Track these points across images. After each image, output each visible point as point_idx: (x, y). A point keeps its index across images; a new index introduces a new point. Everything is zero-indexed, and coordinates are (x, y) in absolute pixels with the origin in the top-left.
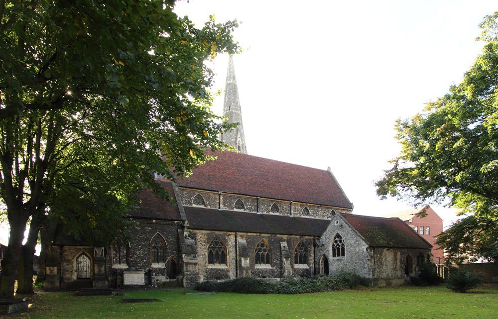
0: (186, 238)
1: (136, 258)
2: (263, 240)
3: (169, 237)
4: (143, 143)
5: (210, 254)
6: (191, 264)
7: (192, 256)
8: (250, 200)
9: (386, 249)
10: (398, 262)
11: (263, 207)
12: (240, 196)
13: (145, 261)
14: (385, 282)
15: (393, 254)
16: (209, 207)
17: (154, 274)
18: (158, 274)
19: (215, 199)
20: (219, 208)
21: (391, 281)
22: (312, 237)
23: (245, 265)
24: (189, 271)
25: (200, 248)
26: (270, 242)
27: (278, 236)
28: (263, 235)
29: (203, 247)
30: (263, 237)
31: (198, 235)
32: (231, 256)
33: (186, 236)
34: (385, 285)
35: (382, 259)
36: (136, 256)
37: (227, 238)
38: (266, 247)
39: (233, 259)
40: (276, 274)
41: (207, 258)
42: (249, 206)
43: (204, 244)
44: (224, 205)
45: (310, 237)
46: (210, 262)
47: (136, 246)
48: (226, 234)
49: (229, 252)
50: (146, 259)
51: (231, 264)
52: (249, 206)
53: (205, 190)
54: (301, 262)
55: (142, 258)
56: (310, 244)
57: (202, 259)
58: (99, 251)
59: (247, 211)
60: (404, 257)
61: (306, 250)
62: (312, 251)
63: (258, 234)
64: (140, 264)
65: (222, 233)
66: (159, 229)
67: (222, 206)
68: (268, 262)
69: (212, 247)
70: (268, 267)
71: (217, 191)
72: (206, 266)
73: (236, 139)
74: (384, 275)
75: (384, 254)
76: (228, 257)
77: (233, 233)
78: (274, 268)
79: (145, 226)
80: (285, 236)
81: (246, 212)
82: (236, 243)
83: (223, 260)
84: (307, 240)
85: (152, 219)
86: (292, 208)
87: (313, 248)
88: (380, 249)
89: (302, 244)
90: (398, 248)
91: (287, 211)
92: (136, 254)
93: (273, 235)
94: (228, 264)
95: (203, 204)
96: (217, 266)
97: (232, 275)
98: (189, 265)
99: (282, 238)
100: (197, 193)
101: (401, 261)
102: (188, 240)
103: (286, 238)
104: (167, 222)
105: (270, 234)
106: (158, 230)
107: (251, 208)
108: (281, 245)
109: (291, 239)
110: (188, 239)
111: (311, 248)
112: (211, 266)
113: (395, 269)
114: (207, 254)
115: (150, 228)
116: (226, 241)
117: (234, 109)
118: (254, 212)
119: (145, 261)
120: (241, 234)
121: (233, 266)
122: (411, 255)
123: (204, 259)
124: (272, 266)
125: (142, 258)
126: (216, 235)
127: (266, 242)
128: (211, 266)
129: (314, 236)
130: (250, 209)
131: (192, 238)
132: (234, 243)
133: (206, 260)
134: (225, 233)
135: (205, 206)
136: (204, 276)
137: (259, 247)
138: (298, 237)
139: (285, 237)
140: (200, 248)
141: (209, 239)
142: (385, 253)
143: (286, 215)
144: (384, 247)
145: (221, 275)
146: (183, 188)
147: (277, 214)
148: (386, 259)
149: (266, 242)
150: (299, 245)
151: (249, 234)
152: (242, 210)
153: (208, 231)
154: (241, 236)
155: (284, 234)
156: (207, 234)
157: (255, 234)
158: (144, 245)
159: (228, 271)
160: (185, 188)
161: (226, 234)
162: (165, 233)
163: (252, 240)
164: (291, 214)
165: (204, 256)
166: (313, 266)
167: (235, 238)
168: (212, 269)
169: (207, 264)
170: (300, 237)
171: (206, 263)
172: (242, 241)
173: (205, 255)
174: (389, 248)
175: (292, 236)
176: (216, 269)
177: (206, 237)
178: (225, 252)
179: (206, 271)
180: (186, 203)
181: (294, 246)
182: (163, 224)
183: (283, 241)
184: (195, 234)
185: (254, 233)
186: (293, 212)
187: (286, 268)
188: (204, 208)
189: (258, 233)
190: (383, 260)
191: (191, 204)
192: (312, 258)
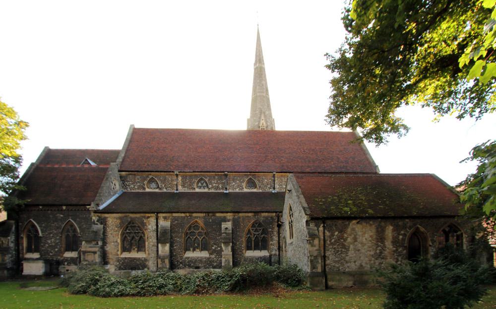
0: (95, 224)
1: (48, 247)
2: (196, 221)
3: (83, 223)
4: (465, 202)
5: (124, 240)
6: (89, 252)
7: (94, 243)
8: (216, 177)
9: (354, 222)
10: (389, 244)
11: (234, 183)
12: (201, 174)
13: (56, 250)
14: (351, 278)
15: (374, 230)
16: (165, 190)
17: (66, 263)
18: (70, 263)
19: (172, 180)
20: (177, 190)
21: (366, 278)
22: (274, 214)
23: (163, 252)
24: (86, 261)
25: (111, 234)
26: (206, 223)
27: (218, 215)
28: (194, 215)
29: (115, 233)
30: (196, 217)
31: (109, 219)
32: (151, 239)
33: (94, 221)
34: (351, 283)
35: (345, 240)
36: (47, 245)
37: (145, 221)
38: (202, 229)
39: (153, 246)
40: (215, 264)
41: (120, 246)
42: (214, 185)
43: (116, 229)
44: (183, 186)
45: (270, 214)
46: (124, 249)
47: (47, 235)
48: (144, 217)
49: (148, 238)
50: (57, 248)
51: (150, 252)
52: (214, 185)
53: (158, 172)
54: (257, 248)
55: (53, 247)
56: (271, 223)
57: (113, 247)
58: (6, 241)
59: (213, 191)
60: (404, 235)
61: (265, 231)
62: (275, 233)
63: (188, 214)
64: (52, 253)
65: (138, 215)
66: (71, 216)
67: (180, 187)
68: (204, 248)
69: (127, 233)
70: (205, 254)
71: (173, 172)
72: (118, 255)
73: (259, 122)
74: (353, 267)
75: (349, 230)
76: (147, 243)
77: (152, 215)
78: (213, 256)
79: (56, 214)
80: (229, 214)
81: (210, 191)
82: (157, 226)
83: (141, 247)
84: (267, 218)
85: (62, 205)
86: (276, 181)
87: (276, 229)
88: (340, 222)
89: (257, 225)
90: (385, 218)
91: (269, 186)
92: (48, 243)
93: (210, 214)
94: (147, 252)
95: (158, 187)
96: (134, 255)
97: (153, 265)
98: (86, 254)
99: (225, 217)
100: (151, 177)
101: (395, 242)
102: (96, 226)
103: (231, 218)
104: (78, 208)
105: (206, 213)
106: (70, 217)
107: (218, 187)
108: (223, 226)
109: (239, 218)
110: (97, 224)
111: (273, 228)
112: (126, 255)
113: (380, 256)
114: (119, 241)
115: (62, 216)
116: (144, 224)
117: (259, 92)
118: (221, 191)
119: (56, 250)
120: (164, 215)
121: (154, 255)
122: (422, 229)
123: (115, 246)
124: (211, 254)
125: (53, 247)
126: (131, 218)
127: (201, 223)
128: (126, 255)
129: (276, 212)
130: (217, 188)
131: (101, 224)
132: (155, 227)
133: (118, 248)
134: (142, 215)
135: (160, 189)
136: (116, 266)
137: (192, 230)
138: (250, 214)
139: (229, 216)
140: (111, 234)
141: (122, 223)
142: (353, 229)
143: (267, 190)
144: (350, 218)
145: (138, 265)
146: (134, 173)
147: (255, 190)
148: (355, 239)
149: (201, 223)
150: (253, 226)
151: (174, 215)
152: (206, 190)
153: (120, 215)
154: (165, 218)
155: (227, 212)
156: (120, 218)
157: (183, 215)
158: (55, 234)
159: (146, 260)
160: (136, 173)
161: (144, 217)
162: (78, 219)
163: (179, 222)
164: (274, 188)
165: (116, 244)
166: (277, 253)
167: (156, 221)
168: (126, 258)
169: (119, 253)
170: (253, 214)
171: (118, 251)
172: (165, 224)
173: (117, 241)
174: (361, 218)
175: (241, 215)
176: (131, 258)
177: (118, 221)
178: (144, 238)
179: (118, 261)
180: (138, 189)
181: (244, 227)
182: (75, 210)
183: (225, 220)
184: (106, 218)
185: (181, 213)
186: (277, 186)
187: (223, 256)
188: (159, 191)
189: (186, 212)
190: (349, 240)
191: (144, 189)
192: (275, 242)
